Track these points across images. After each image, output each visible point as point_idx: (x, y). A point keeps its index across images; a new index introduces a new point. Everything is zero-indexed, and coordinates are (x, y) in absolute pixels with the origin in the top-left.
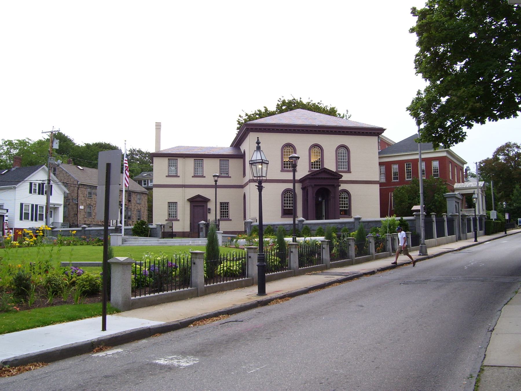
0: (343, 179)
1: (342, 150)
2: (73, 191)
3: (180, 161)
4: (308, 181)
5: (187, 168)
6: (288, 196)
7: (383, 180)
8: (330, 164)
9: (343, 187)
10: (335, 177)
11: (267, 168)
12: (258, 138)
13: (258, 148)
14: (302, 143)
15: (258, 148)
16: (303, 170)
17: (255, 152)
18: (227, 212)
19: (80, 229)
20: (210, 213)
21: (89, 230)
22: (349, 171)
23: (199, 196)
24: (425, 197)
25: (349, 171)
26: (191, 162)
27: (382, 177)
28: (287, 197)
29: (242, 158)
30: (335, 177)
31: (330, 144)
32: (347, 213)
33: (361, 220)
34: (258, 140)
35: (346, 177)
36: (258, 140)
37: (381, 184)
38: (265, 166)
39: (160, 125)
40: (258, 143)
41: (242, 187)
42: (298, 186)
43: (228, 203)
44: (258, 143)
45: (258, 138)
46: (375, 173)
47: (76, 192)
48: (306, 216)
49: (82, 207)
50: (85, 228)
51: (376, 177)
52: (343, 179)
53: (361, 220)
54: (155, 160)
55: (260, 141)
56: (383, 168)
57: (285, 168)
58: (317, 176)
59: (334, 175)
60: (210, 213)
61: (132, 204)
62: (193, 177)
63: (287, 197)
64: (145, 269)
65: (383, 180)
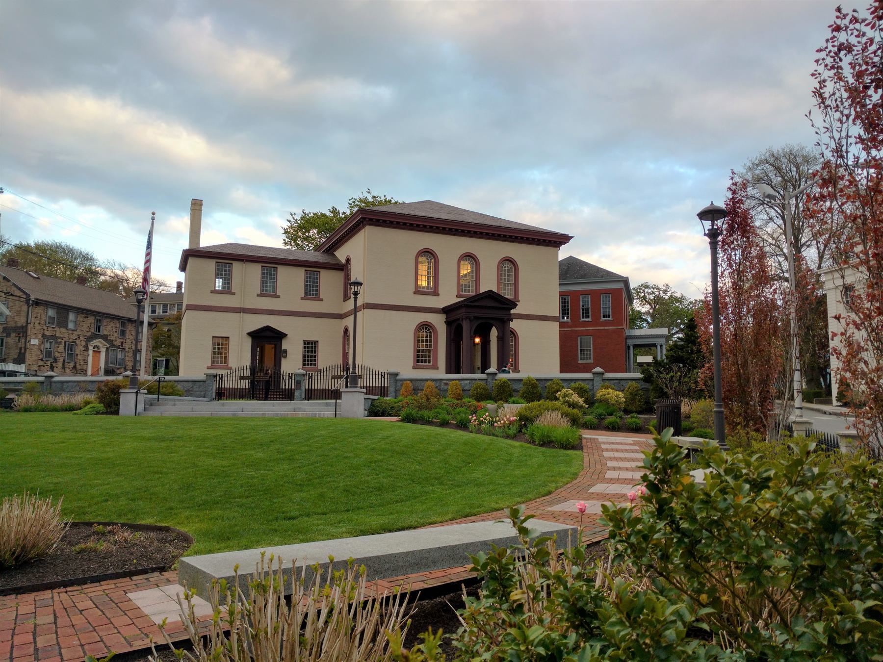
2: (18, 313)
3: (237, 267)
4: (463, 310)
5: (248, 277)
18: (315, 356)
19: (41, 379)
20: (285, 357)
21: (62, 382)
23: (268, 329)
26: (256, 270)
29: (342, 270)
31: (490, 253)
32: (516, 370)
33: (399, 377)
39: (201, 205)
41: (341, 316)
42: (439, 322)
43: (316, 342)
47: (24, 314)
48: (449, 371)
49: (34, 342)
50: (52, 377)
51: (555, 312)
53: (399, 377)
59: (503, 303)
60: (285, 357)
61: (128, 341)
62: (258, 295)
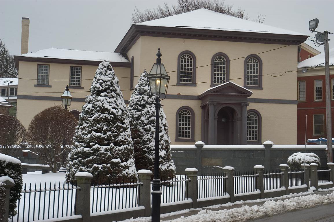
0: (252, 97)
1: (253, 62)
6: (184, 115)
7: (303, 99)
8: (237, 77)
9: (252, 106)
10: (243, 95)
11: (167, 83)
12: (159, 49)
13: (159, 61)
14: (204, 53)
15: (159, 61)
16: (203, 85)
17: (155, 66)
22: (260, 87)
24: (323, 98)
25: (260, 87)
27: (302, 96)
28: (183, 117)
30: (243, 95)
31: (237, 55)
34: (159, 52)
35: (256, 94)
36: (159, 52)
37: (300, 105)
38: (163, 81)
40: (159, 55)
44: (159, 55)
45: (159, 49)
46: (291, 90)
52: (252, 97)
53: (69, 86)
54: (21, 64)
55: (161, 53)
56: (304, 85)
57: (181, 80)
58: (218, 93)
63: (183, 117)
64: (269, 209)
65: (303, 99)
